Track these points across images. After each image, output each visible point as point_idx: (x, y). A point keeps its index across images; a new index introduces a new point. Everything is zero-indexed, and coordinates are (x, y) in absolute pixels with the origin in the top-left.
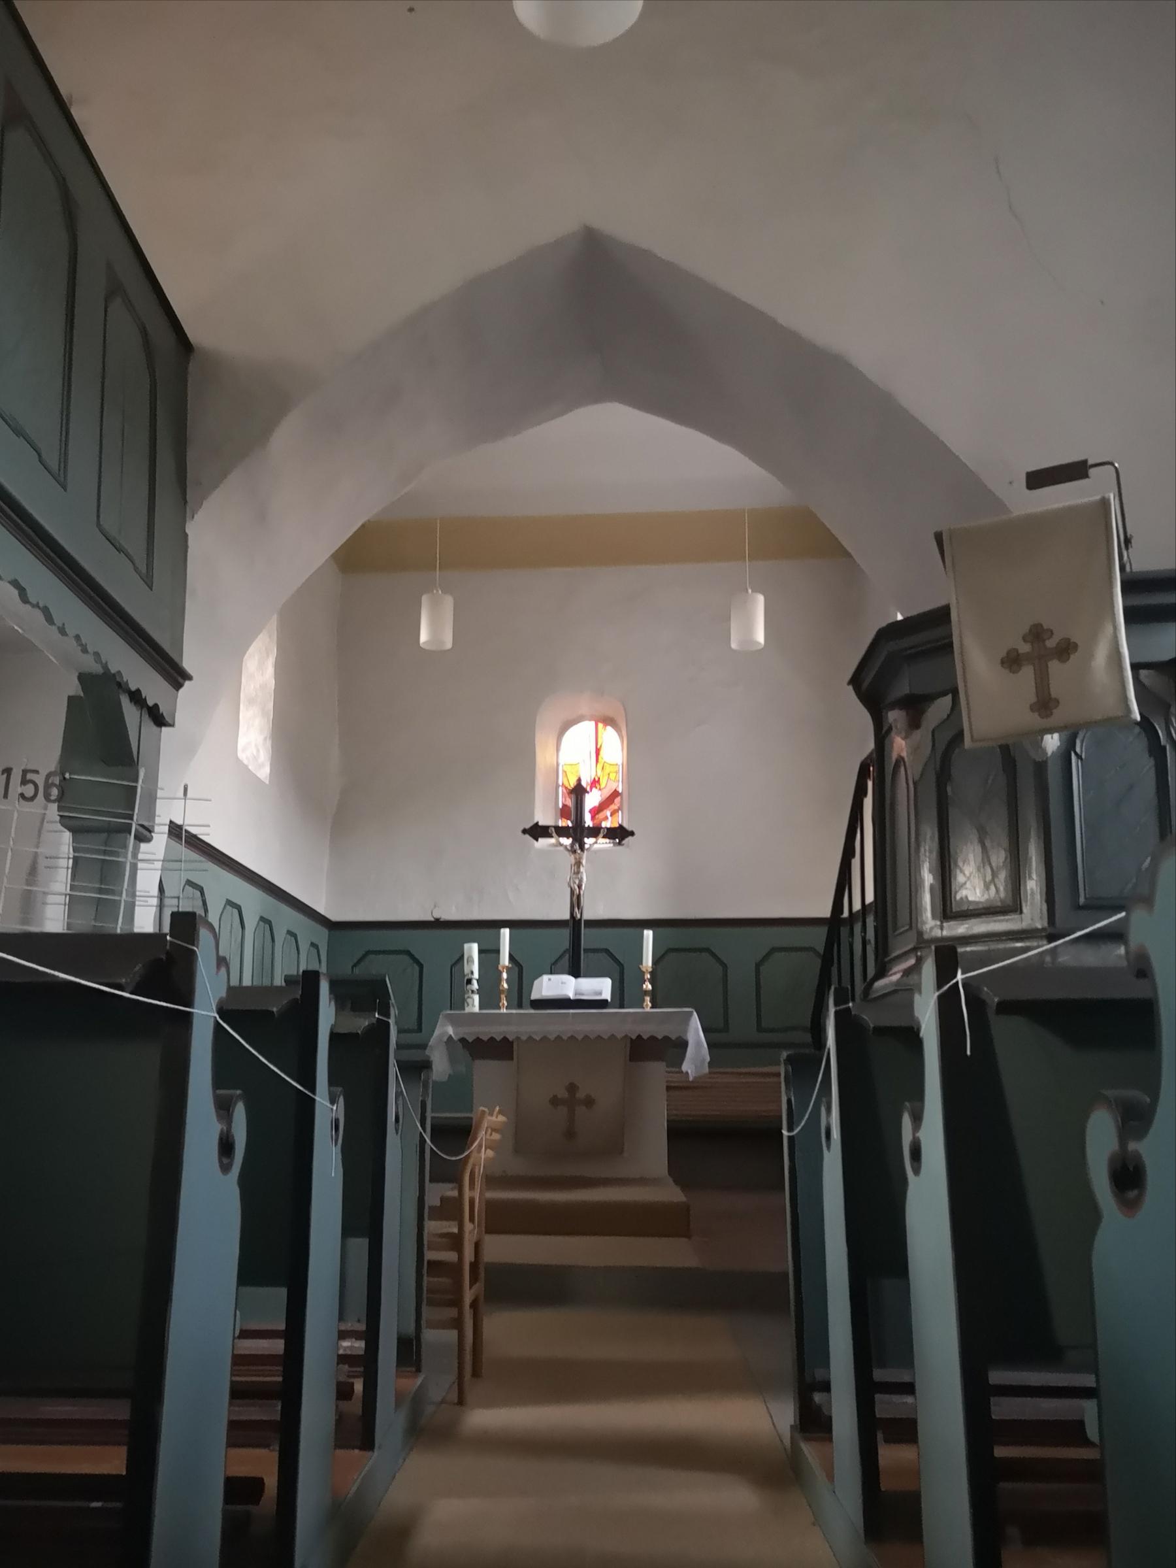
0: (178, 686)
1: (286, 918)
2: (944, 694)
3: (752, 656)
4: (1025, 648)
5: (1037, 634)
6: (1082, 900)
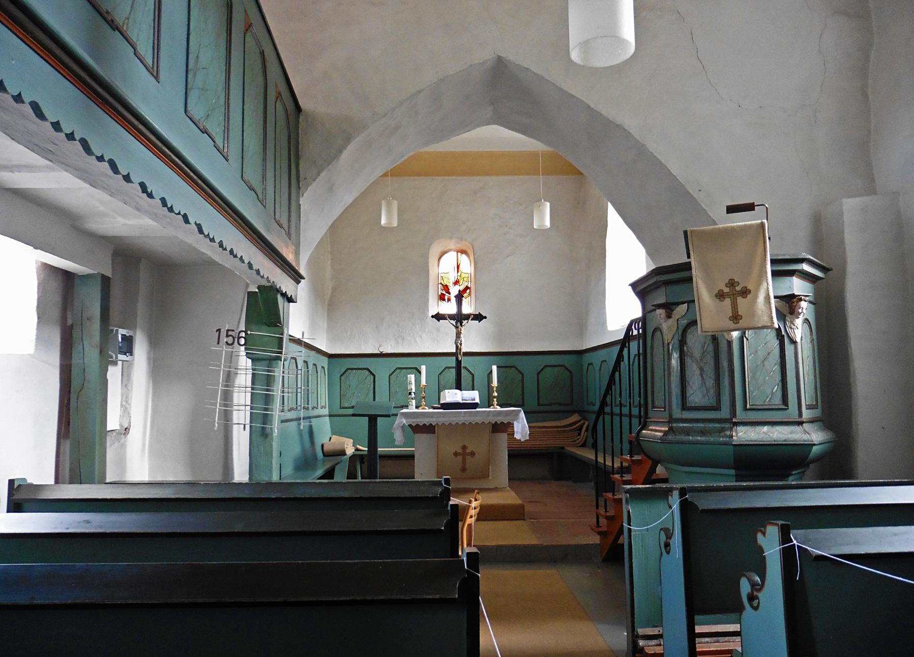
0: (298, 282)
1: (313, 357)
2: (683, 303)
3: (543, 232)
4: (726, 290)
5: (732, 284)
6: (748, 406)
